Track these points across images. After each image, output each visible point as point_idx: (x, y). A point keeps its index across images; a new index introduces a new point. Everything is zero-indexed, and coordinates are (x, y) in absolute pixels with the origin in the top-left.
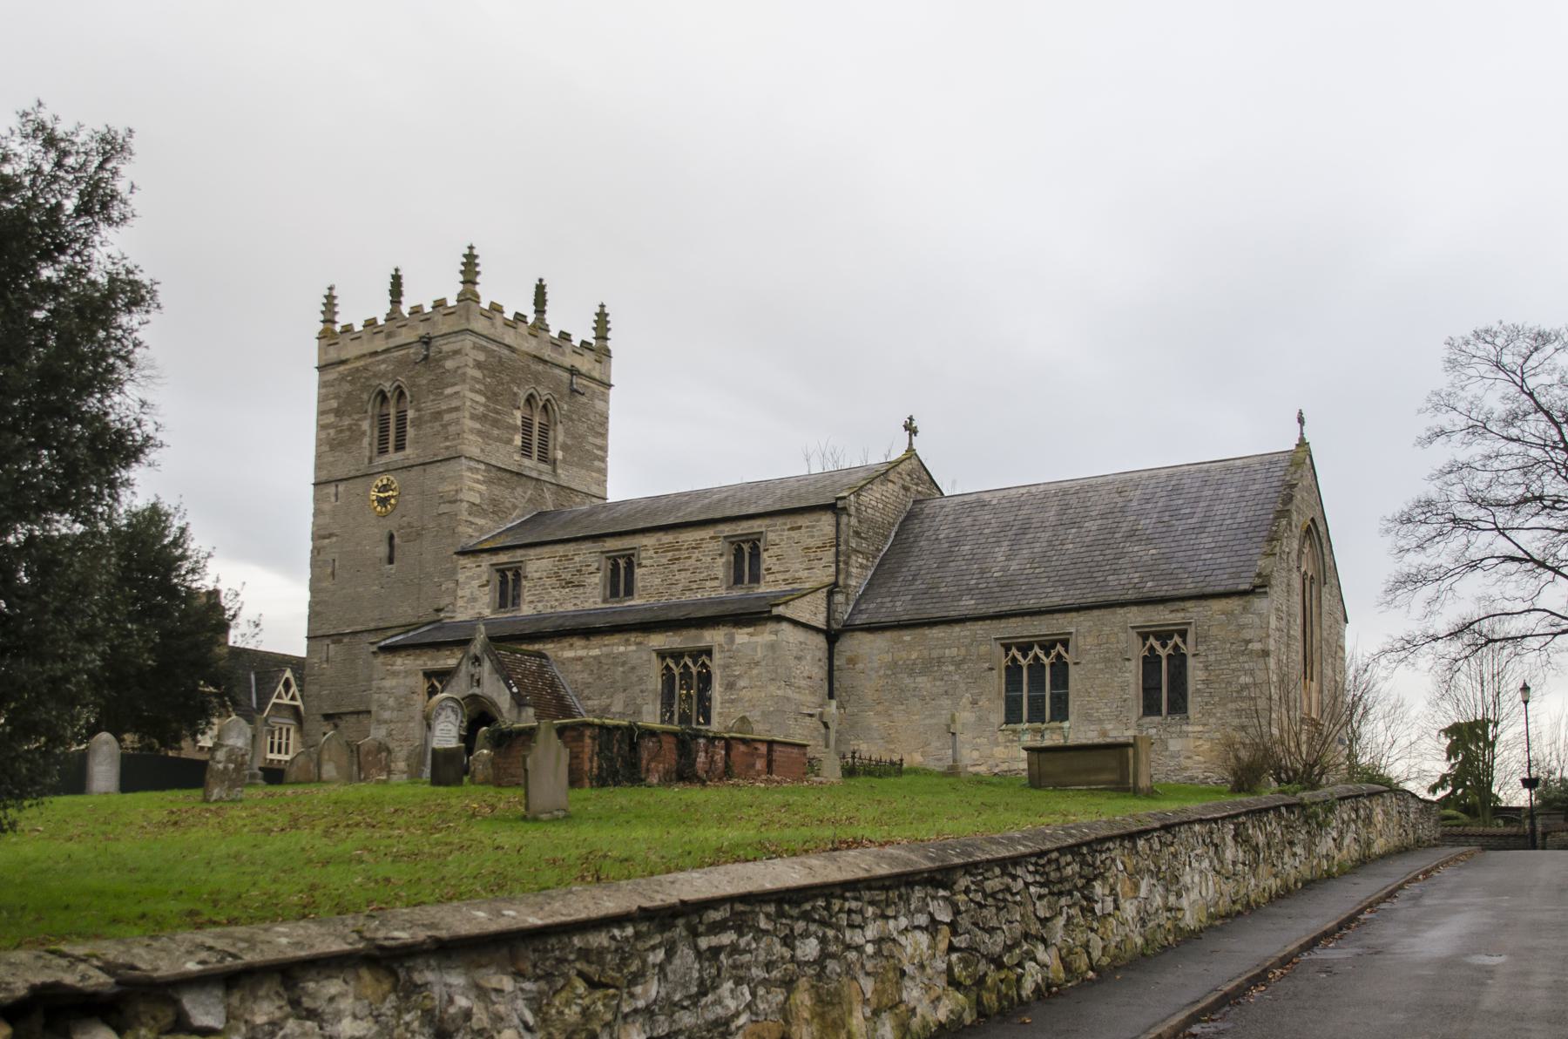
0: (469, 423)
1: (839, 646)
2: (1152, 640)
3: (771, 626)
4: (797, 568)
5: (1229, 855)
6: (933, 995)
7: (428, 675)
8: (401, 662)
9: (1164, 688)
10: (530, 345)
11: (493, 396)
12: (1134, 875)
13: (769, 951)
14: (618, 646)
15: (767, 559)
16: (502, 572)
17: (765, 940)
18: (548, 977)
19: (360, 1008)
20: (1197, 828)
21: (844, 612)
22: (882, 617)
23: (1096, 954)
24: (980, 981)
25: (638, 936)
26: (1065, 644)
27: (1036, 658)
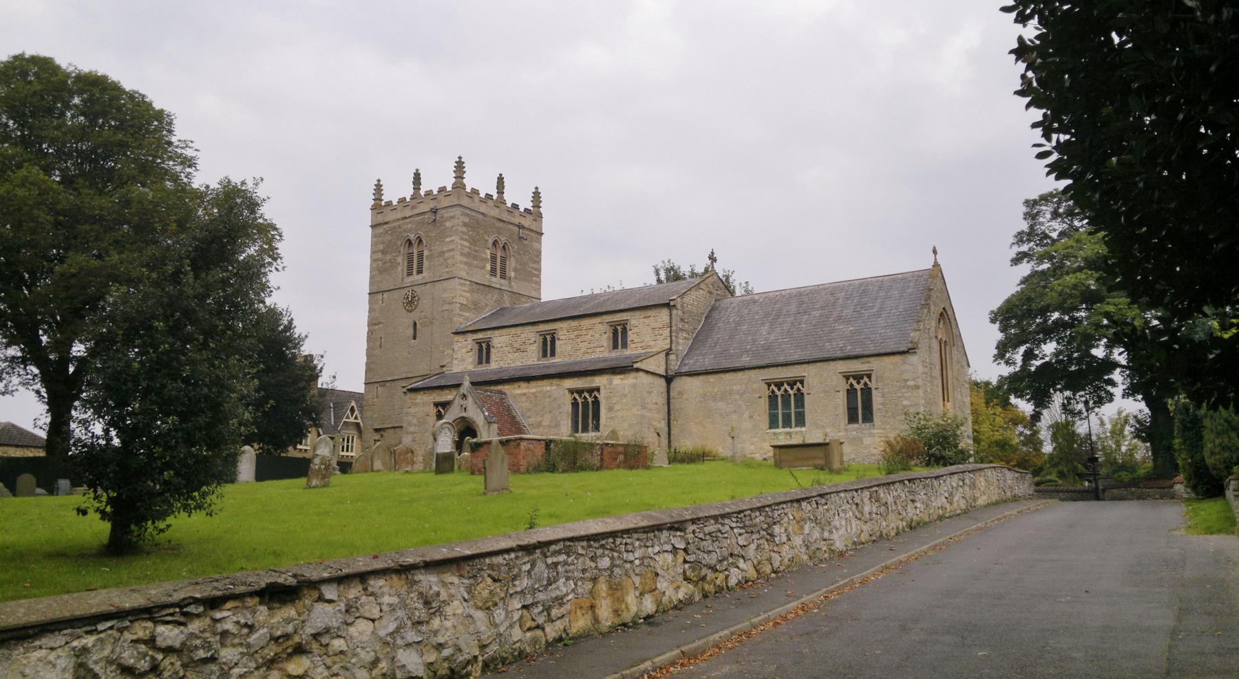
0: (459, 257)
1: (673, 385)
2: (851, 380)
3: (633, 374)
4: (648, 339)
5: (867, 509)
6: (675, 585)
7: (436, 405)
8: (420, 398)
9: (860, 407)
10: (494, 212)
11: (474, 242)
12: (801, 522)
13: (584, 563)
14: (546, 387)
15: (631, 336)
16: (480, 344)
17: (581, 559)
18: (474, 577)
19: (393, 591)
20: (842, 495)
21: (675, 365)
22: (697, 368)
23: (776, 564)
24: (703, 579)
25: (517, 557)
26: (802, 382)
27: (786, 390)
